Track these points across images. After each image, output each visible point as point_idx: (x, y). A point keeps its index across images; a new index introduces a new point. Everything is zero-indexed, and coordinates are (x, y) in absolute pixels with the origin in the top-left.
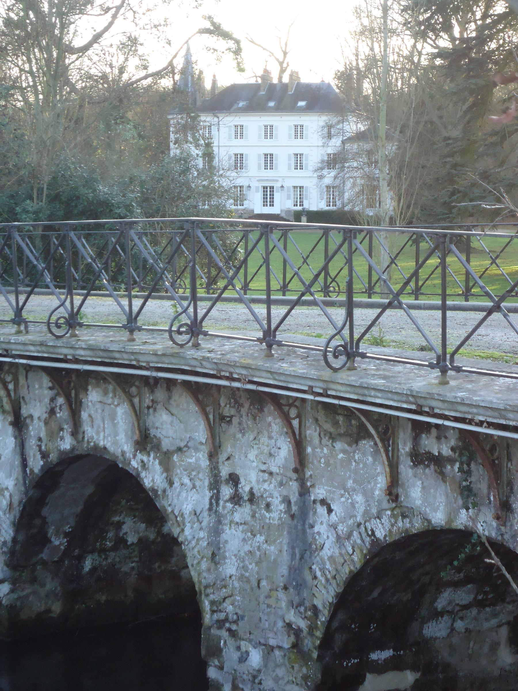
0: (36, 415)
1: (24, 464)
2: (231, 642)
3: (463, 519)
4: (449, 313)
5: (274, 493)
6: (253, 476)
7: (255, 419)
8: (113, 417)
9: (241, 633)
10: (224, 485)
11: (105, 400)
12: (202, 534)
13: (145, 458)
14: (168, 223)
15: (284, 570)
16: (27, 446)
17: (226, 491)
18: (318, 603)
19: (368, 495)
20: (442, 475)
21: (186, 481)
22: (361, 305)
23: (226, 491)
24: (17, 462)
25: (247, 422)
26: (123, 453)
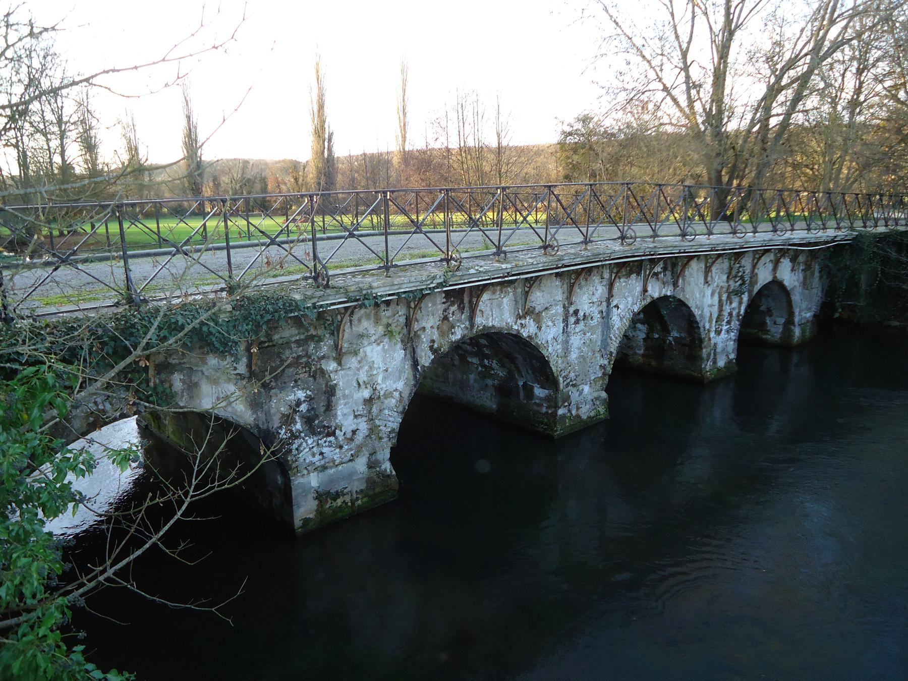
0: (428, 326)
1: (415, 363)
2: (574, 390)
3: (664, 292)
4: (389, 237)
5: (595, 312)
6: (586, 307)
7: (586, 280)
8: (499, 306)
9: (578, 383)
10: (571, 315)
11: (494, 297)
12: (559, 347)
13: (523, 322)
14: (756, 181)
15: (599, 343)
16: (418, 351)
17: (572, 320)
18: (612, 350)
19: (633, 296)
20: (658, 279)
21: (550, 323)
22: (322, 239)
23: (572, 320)
24: (408, 365)
25: (583, 283)
26: (507, 324)
